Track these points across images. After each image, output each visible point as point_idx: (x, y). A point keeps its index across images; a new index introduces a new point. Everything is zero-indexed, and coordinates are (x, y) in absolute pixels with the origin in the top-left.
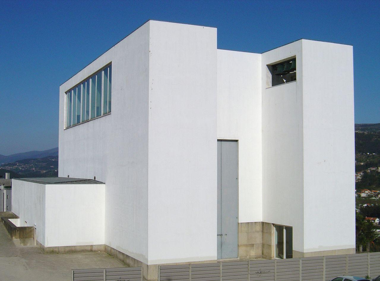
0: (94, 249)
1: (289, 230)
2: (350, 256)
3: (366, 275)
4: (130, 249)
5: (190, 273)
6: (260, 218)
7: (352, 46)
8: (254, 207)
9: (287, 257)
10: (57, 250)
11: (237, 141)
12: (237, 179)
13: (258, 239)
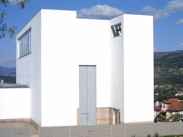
0: (25, 120)
1: (117, 111)
2: (152, 124)
3: (148, 134)
4: (36, 121)
5: (125, 128)
6: (109, 106)
7: (153, 16)
8: (104, 100)
9: (119, 124)
10: (6, 121)
11: (95, 66)
12: (96, 85)
13: (107, 116)
